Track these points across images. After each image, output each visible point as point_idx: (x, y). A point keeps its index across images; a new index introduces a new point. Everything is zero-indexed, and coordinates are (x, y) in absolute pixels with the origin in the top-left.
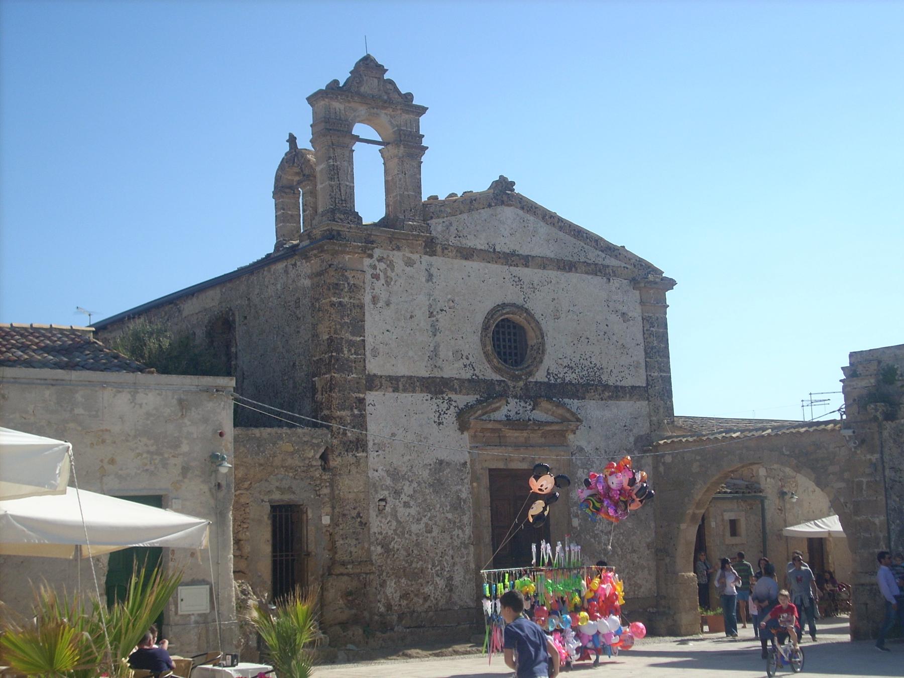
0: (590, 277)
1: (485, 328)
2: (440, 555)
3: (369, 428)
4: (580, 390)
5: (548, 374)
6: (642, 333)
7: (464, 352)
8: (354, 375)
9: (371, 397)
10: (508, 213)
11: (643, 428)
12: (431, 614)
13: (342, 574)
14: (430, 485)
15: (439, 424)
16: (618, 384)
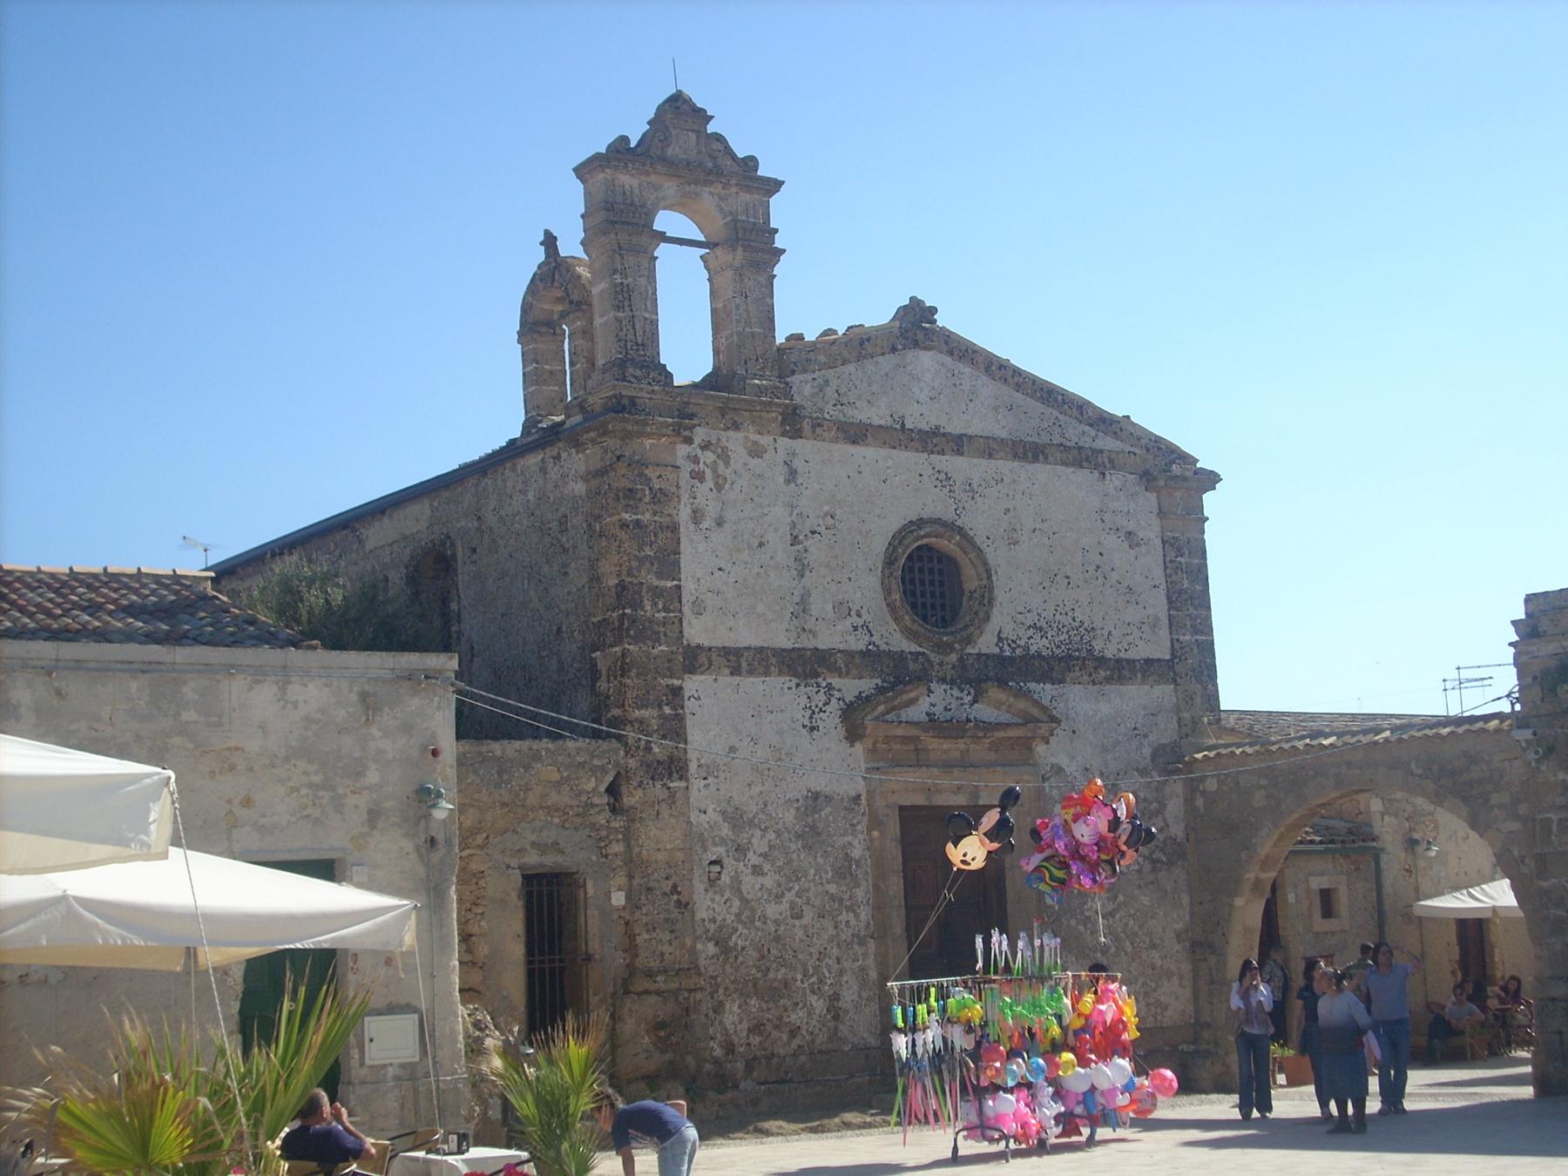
1: (889, 561)
2: (816, 956)
3: (690, 738)
4: (1055, 668)
5: (1000, 639)
7: (854, 604)
8: (663, 648)
9: (693, 684)
10: (926, 361)
11: (1166, 731)
13: (647, 992)
15: (812, 729)
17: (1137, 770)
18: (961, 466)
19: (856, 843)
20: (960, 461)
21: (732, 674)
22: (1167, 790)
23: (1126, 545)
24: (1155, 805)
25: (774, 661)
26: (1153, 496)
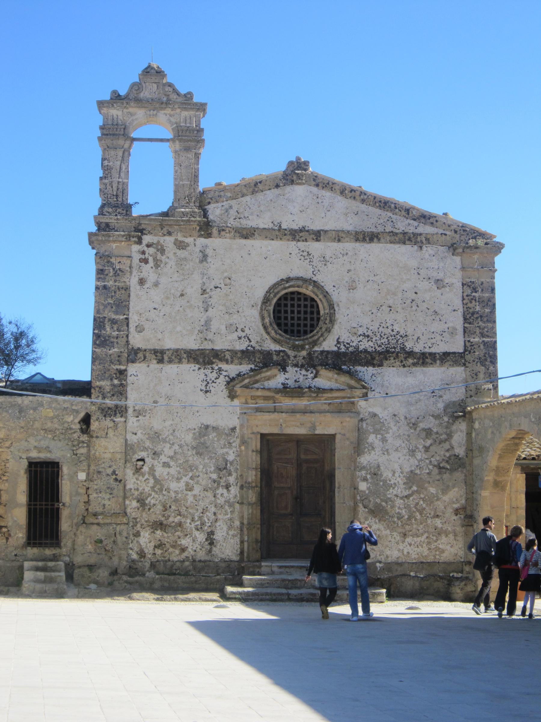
0: (397, 246)
1: (266, 300)
2: (200, 510)
3: (129, 396)
4: (376, 358)
5: (338, 342)
6: (461, 299)
7: (245, 324)
8: (116, 350)
9: (132, 369)
10: (299, 191)
11: (457, 394)
12: (187, 563)
13: (93, 524)
14: (193, 448)
15: (206, 392)
16: (427, 350)
17: (433, 416)
18: (316, 248)
19: (231, 452)
20: (316, 245)
21: (158, 363)
22: (454, 427)
23: (435, 287)
24: (444, 437)
25: (185, 356)
26: (458, 259)
